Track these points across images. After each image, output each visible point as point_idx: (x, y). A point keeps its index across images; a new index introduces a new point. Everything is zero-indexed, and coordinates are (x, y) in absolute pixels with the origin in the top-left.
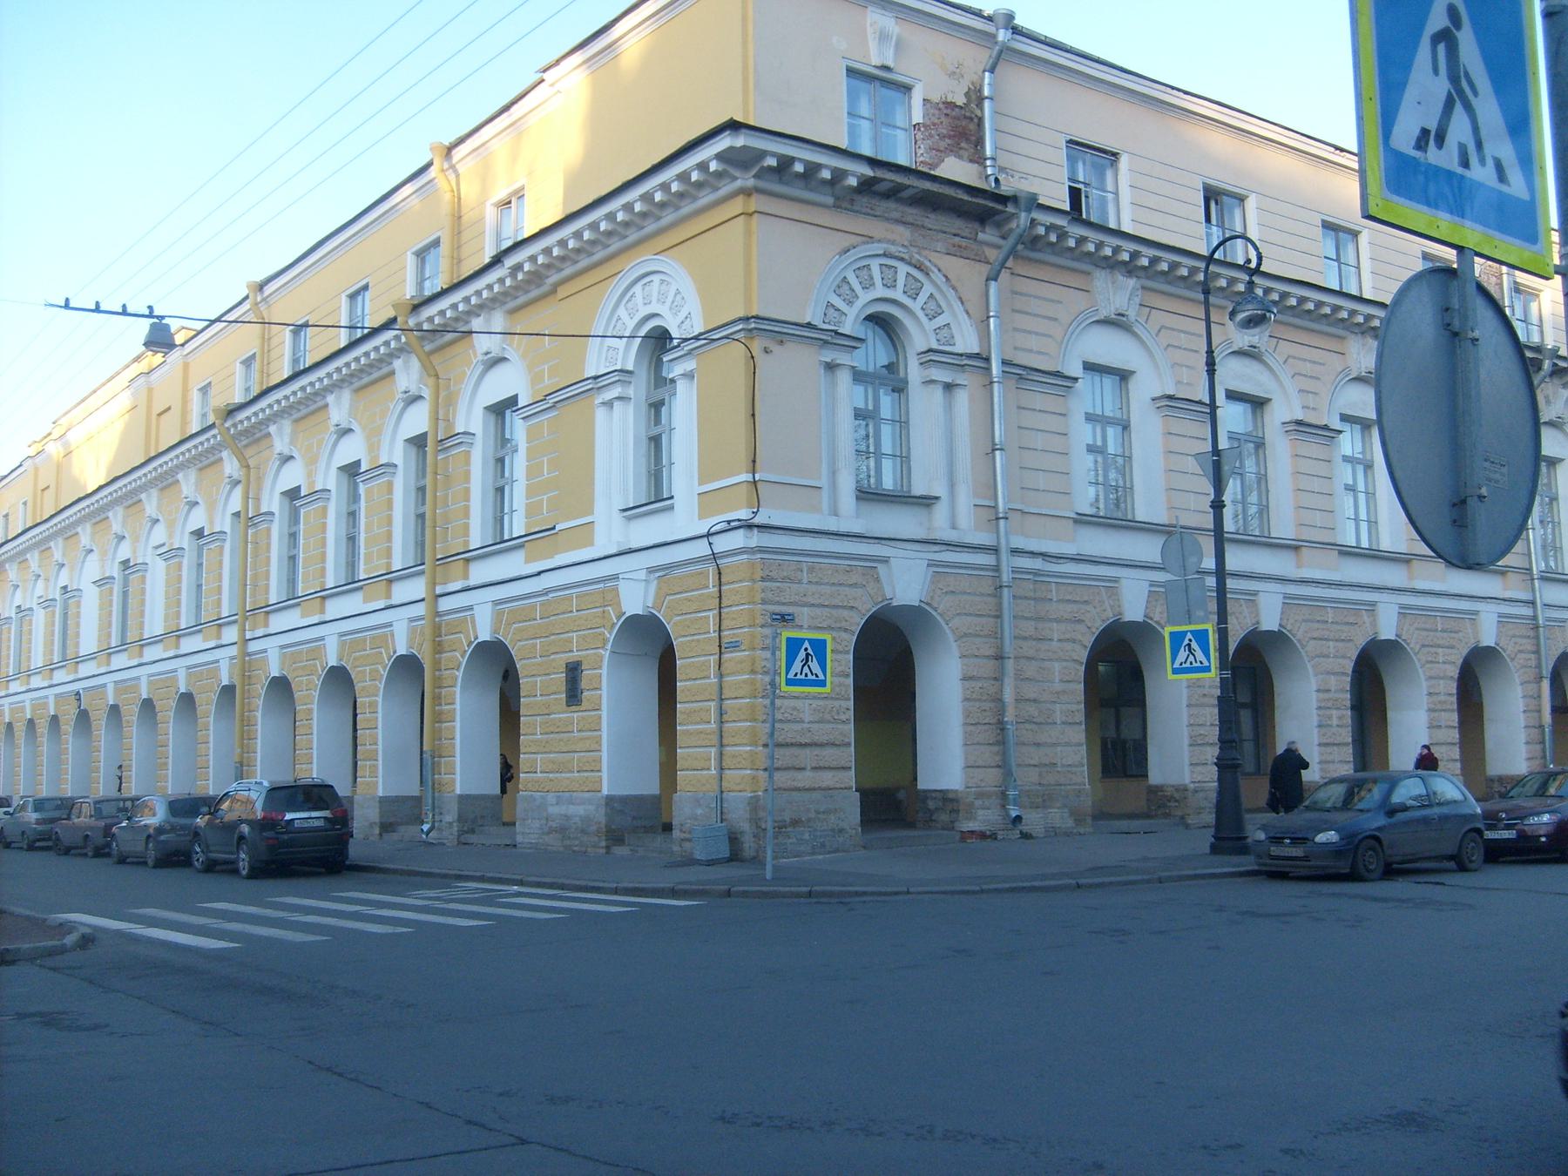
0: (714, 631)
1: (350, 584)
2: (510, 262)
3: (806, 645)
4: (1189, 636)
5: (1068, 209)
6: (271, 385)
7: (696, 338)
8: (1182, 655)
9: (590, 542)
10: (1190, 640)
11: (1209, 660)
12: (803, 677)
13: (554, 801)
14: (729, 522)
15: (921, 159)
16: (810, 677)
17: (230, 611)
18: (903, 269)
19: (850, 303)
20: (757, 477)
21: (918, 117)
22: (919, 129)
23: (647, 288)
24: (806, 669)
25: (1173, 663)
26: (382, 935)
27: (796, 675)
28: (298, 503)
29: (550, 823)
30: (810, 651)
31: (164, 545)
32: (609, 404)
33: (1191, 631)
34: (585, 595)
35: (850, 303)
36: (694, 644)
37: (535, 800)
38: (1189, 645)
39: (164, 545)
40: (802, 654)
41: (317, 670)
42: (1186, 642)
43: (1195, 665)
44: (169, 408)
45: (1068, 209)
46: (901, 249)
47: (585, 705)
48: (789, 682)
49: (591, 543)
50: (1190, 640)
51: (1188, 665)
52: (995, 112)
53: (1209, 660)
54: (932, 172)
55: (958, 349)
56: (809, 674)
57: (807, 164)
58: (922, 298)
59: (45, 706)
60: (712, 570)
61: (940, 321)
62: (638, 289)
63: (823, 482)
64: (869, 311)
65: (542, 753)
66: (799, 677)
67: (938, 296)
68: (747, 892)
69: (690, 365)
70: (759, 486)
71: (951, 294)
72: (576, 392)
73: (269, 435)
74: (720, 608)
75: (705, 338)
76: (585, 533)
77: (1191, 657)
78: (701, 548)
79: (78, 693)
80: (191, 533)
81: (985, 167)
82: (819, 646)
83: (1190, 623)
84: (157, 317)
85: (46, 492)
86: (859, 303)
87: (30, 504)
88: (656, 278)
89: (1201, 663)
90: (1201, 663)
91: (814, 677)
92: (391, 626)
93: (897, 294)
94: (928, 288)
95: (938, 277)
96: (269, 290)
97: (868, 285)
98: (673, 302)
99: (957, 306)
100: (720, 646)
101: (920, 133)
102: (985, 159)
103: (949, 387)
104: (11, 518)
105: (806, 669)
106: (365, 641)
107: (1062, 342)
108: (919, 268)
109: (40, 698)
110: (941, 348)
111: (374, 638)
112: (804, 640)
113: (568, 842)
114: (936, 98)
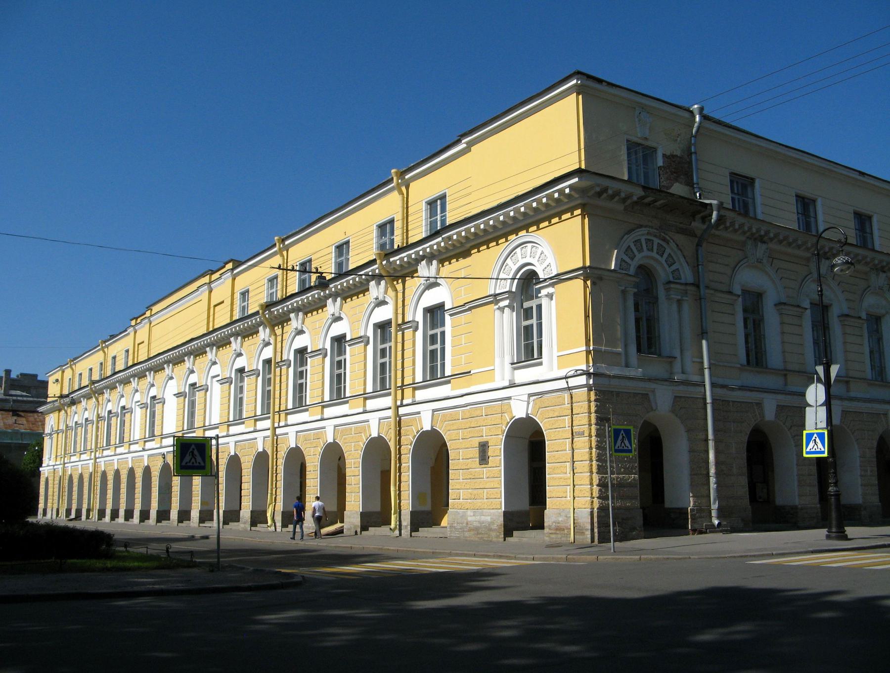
0: (568, 427)
3: (622, 432)
4: (815, 435)
5: (731, 208)
7: (551, 278)
8: (811, 444)
9: (493, 380)
10: (816, 438)
11: (824, 448)
12: (622, 448)
13: (472, 514)
14: (577, 371)
15: (663, 184)
16: (625, 448)
18: (656, 241)
19: (632, 259)
22: (661, 169)
23: (524, 249)
24: (623, 444)
25: (806, 449)
27: (618, 447)
29: (469, 526)
30: (624, 435)
31: (218, 375)
32: (502, 309)
33: (817, 434)
34: (490, 407)
35: (632, 259)
36: (556, 433)
37: (459, 514)
38: (815, 440)
39: (218, 375)
41: (320, 444)
43: (817, 450)
44: (223, 302)
45: (731, 208)
46: (655, 231)
47: (490, 464)
50: (816, 438)
52: (697, 160)
53: (824, 448)
54: (668, 191)
55: (683, 281)
56: (624, 446)
58: (665, 256)
59: (77, 470)
60: (566, 396)
61: (674, 267)
62: (519, 250)
64: (641, 262)
65: (463, 489)
66: (620, 448)
67: (672, 254)
69: (551, 290)
71: (679, 253)
74: (572, 414)
75: (559, 279)
77: (816, 446)
78: (562, 384)
79: (164, 454)
81: (694, 188)
82: (628, 432)
84: (320, 273)
86: (636, 259)
87: (131, 352)
88: (529, 245)
90: (820, 449)
91: (626, 448)
92: (369, 421)
93: (654, 254)
94: (668, 251)
95: (672, 244)
97: (640, 250)
98: (539, 258)
99: (682, 260)
100: (572, 434)
101: (661, 171)
102: (694, 184)
104: (117, 359)
105: (623, 444)
106: (351, 429)
107: (732, 276)
108: (664, 240)
109: (138, 456)
110: (676, 281)
111: (357, 428)
113: (480, 536)
114: (668, 153)
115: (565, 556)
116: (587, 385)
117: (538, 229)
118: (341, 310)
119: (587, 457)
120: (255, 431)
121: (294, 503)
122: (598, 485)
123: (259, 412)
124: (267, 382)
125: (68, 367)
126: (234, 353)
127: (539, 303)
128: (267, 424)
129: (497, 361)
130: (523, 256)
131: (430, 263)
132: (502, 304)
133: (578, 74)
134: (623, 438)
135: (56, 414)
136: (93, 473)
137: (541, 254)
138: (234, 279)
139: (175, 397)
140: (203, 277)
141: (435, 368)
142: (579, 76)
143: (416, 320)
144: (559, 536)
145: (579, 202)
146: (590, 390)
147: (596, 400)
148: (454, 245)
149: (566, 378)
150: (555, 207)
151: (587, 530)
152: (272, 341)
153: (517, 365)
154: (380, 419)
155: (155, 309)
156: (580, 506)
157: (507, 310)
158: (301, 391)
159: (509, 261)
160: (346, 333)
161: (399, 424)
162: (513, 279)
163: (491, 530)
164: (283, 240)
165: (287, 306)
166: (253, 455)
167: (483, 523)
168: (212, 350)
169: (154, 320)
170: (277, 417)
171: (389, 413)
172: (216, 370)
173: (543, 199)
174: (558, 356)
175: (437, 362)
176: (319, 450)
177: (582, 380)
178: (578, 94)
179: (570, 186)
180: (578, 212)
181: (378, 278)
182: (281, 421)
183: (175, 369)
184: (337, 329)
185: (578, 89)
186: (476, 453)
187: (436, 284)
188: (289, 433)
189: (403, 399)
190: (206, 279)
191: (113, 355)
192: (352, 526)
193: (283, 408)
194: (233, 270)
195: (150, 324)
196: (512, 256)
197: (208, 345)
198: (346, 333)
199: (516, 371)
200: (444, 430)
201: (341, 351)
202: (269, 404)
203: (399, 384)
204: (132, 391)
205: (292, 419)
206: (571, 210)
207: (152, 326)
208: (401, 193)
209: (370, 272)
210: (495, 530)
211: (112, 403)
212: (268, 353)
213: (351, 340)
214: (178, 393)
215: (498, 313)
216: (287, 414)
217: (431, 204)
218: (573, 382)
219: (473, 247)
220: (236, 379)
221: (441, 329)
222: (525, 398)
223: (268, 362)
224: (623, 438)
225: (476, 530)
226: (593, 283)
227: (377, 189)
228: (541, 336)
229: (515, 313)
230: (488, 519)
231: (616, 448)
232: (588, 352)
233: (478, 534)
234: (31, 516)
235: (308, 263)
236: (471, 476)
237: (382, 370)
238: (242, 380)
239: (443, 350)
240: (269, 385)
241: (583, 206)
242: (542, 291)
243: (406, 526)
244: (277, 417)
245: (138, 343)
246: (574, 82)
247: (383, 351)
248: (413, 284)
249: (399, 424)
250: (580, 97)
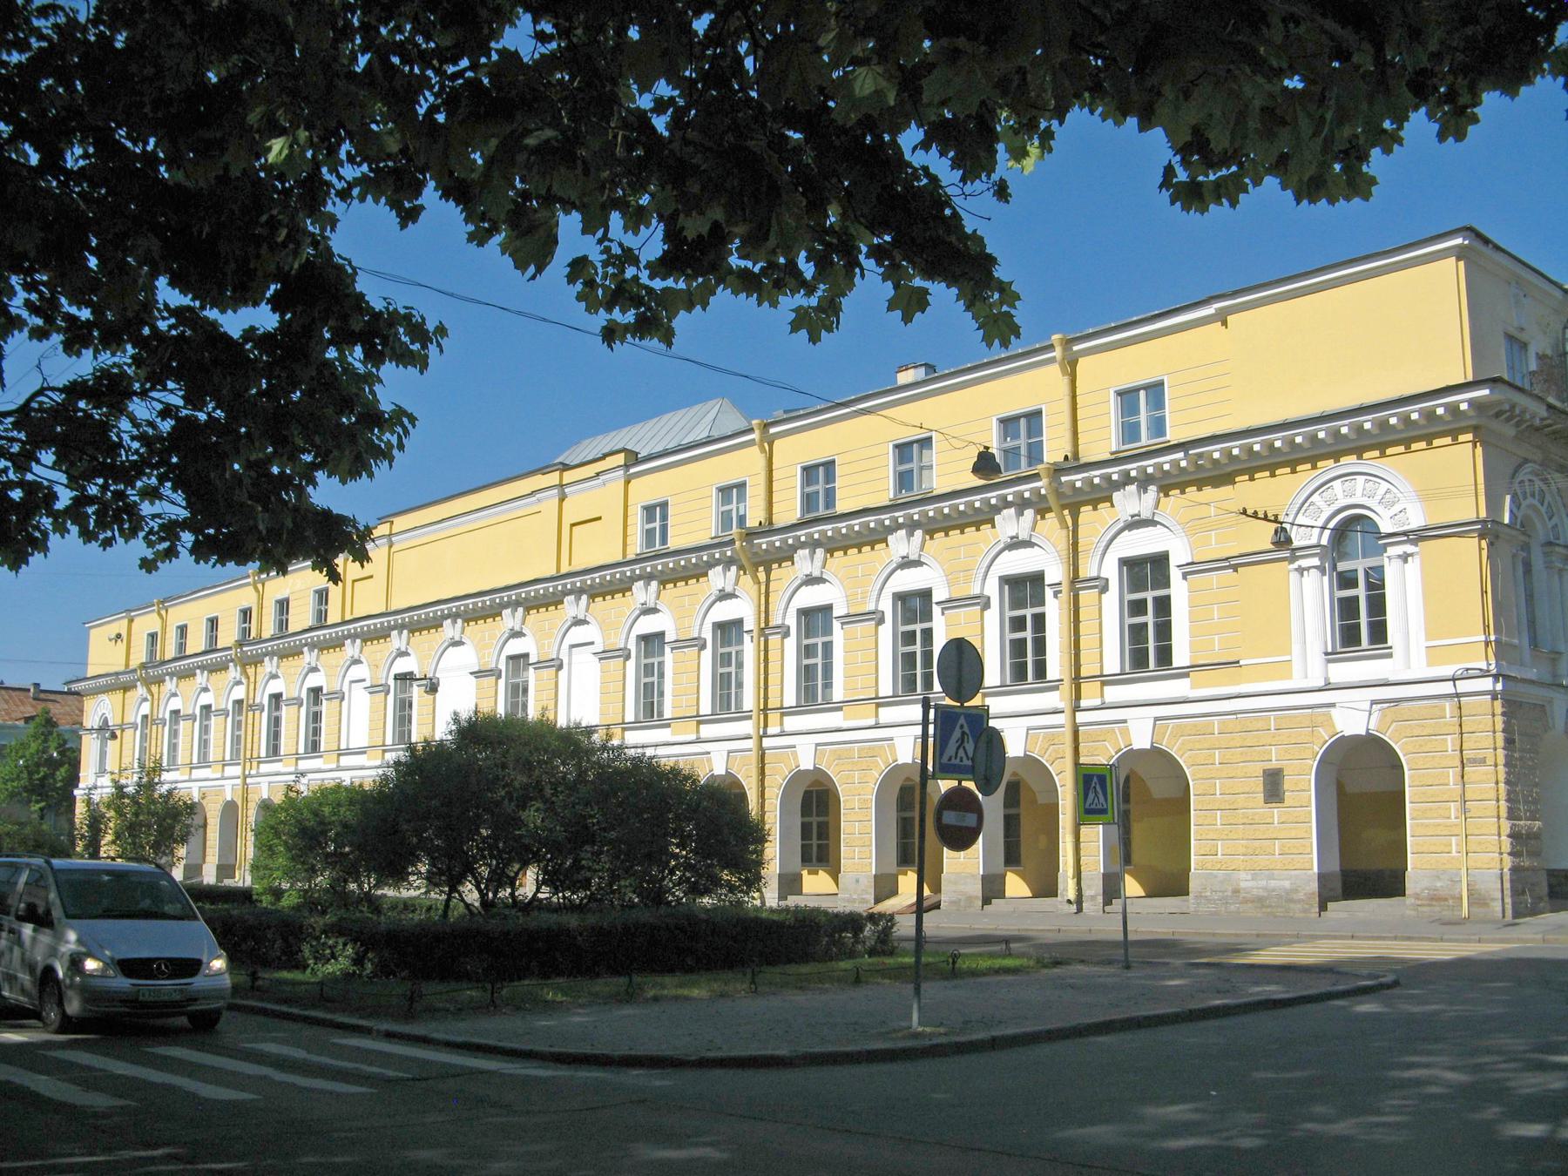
3: (962, 721)
12: (958, 761)
13: (1249, 877)
17: (845, 696)
21: (1533, 366)
27: (950, 759)
30: (966, 729)
32: (1301, 570)
40: (957, 734)
44: (600, 518)
47: (1287, 802)
49: (1290, 677)
66: (953, 761)
76: (1284, 669)
78: (1447, 688)
105: (961, 752)
115: (1540, 936)
116: (1494, 695)
117: (1383, 455)
119: (1493, 795)
120: (223, 778)
122: (1509, 836)
123: (228, 757)
124: (237, 725)
125: (248, 584)
128: (235, 771)
131: (727, 568)
132: (1304, 563)
133: (1469, 230)
135: (119, 695)
138: (628, 482)
139: (472, 677)
142: (1468, 233)
143: (986, 593)
144: (1437, 909)
145: (1474, 422)
146: (1494, 698)
147: (1503, 714)
149: (1454, 679)
150: (1424, 427)
151: (1494, 900)
152: (244, 680)
153: (1331, 656)
154: (729, 752)
155: (401, 523)
156: (1479, 865)
157: (1314, 573)
158: (239, 743)
161: (1076, 733)
162: (1323, 528)
163: (1292, 901)
164: (766, 426)
167: (1273, 890)
168: (202, 673)
169: (400, 541)
170: (248, 764)
171: (749, 744)
172: (356, 672)
176: (219, 807)
177: (1487, 684)
178: (1458, 259)
180: (1469, 437)
182: (1083, 694)
183: (412, 639)
184: (314, 680)
185: (1460, 253)
186: (1258, 786)
187: (732, 596)
189: (766, 726)
190: (553, 478)
191: (280, 596)
192: (963, 898)
193: (255, 755)
194: (627, 466)
195: (390, 547)
197: (349, 636)
199: (1330, 665)
200: (1179, 749)
202: (238, 751)
203: (248, 756)
205: (264, 768)
206: (1454, 434)
207: (393, 550)
208: (762, 450)
210: (1299, 901)
212: (239, 693)
214: (848, 616)
215: (1294, 576)
216: (259, 763)
217: (809, 472)
218: (1463, 686)
219: (1241, 472)
220: (638, 652)
221: (660, 659)
222: (1367, 706)
223: (239, 703)
225: (1260, 901)
226: (1491, 545)
229: (1326, 579)
230: (1287, 884)
232: (1487, 643)
233: (1263, 906)
234: (837, 915)
236: (1245, 821)
237: (236, 740)
239: (661, 684)
240: (239, 729)
241: (1475, 429)
242: (1389, 549)
243: (1093, 898)
244: (248, 764)
246: (1459, 241)
248: (784, 576)
249: (1076, 733)
250: (1462, 264)
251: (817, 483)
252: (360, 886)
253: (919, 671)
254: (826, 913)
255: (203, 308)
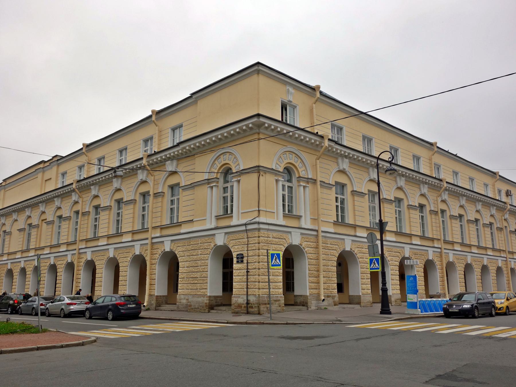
1: (117, 234)
2: (182, 146)
3: (275, 255)
4: (374, 260)
6: (45, 192)
8: (372, 266)
10: (375, 261)
12: (275, 264)
16: (277, 264)
20: (260, 209)
26: (158, 334)
27: (273, 263)
28: (31, 227)
30: (276, 257)
33: (375, 259)
38: (374, 262)
42: (374, 261)
43: (375, 267)
48: (272, 265)
50: (375, 261)
51: (374, 267)
56: (277, 263)
57: (281, 128)
63: (276, 212)
66: (274, 264)
68: (271, 323)
70: (261, 212)
72: (204, 182)
73: (91, 189)
78: (243, 228)
80: (57, 216)
83: (375, 257)
85: (47, 182)
88: (228, 154)
89: (377, 267)
90: (377, 267)
91: (278, 264)
96: (8, 182)
98: (233, 161)
103: (304, 187)
112: (274, 254)
118: (177, 168)
121: (35, 292)
126: (56, 207)
127: (231, 185)
129: (208, 215)
130: (229, 159)
134: (276, 259)
136: (367, 228)
137: (234, 159)
140: (39, 164)
141: (144, 223)
148: (186, 152)
149: (246, 225)
159: (216, 162)
160: (179, 183)
165: (153, 160)
166: (32, 267)
173: (225, 134)
174: (242, 213)
175: (174, 214)
179: (252, 123)
181: (143, 168)
188: (135, 246)
196: (218, 159)
197: (41, 202)
198: (179, 183)
201: (97, 213)
204: (1, 224)
209: (134, 166)
211: (328, 137)
213: (126, 201)
215: (209, 189)
218: (249, 227)
224: (276, 259)
227: (164, 111)
228: (178, 213)
231: (272, 264)
235: (124, 151)
238: (77, 218)
245: (45, 180)
247: (118, 214)
251: (227, 192)
252: (410, 262)
253: (97, 231)
254: (93, 340)
255: (237, 179)
